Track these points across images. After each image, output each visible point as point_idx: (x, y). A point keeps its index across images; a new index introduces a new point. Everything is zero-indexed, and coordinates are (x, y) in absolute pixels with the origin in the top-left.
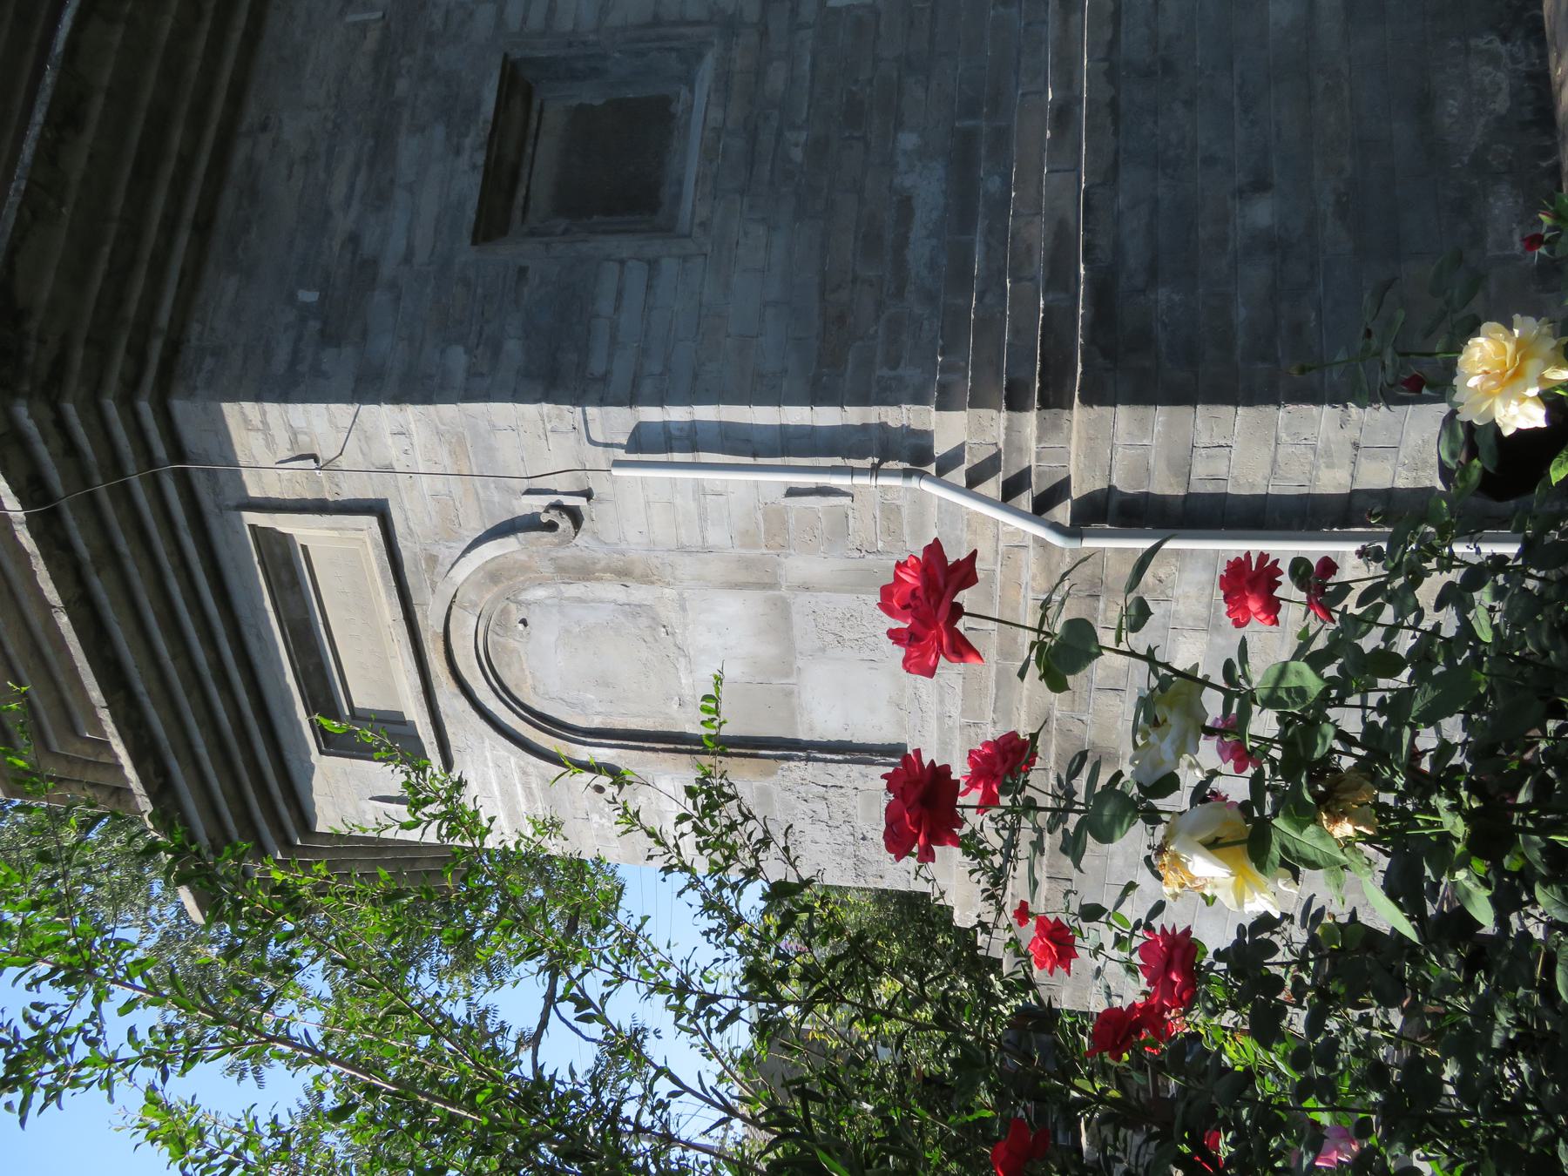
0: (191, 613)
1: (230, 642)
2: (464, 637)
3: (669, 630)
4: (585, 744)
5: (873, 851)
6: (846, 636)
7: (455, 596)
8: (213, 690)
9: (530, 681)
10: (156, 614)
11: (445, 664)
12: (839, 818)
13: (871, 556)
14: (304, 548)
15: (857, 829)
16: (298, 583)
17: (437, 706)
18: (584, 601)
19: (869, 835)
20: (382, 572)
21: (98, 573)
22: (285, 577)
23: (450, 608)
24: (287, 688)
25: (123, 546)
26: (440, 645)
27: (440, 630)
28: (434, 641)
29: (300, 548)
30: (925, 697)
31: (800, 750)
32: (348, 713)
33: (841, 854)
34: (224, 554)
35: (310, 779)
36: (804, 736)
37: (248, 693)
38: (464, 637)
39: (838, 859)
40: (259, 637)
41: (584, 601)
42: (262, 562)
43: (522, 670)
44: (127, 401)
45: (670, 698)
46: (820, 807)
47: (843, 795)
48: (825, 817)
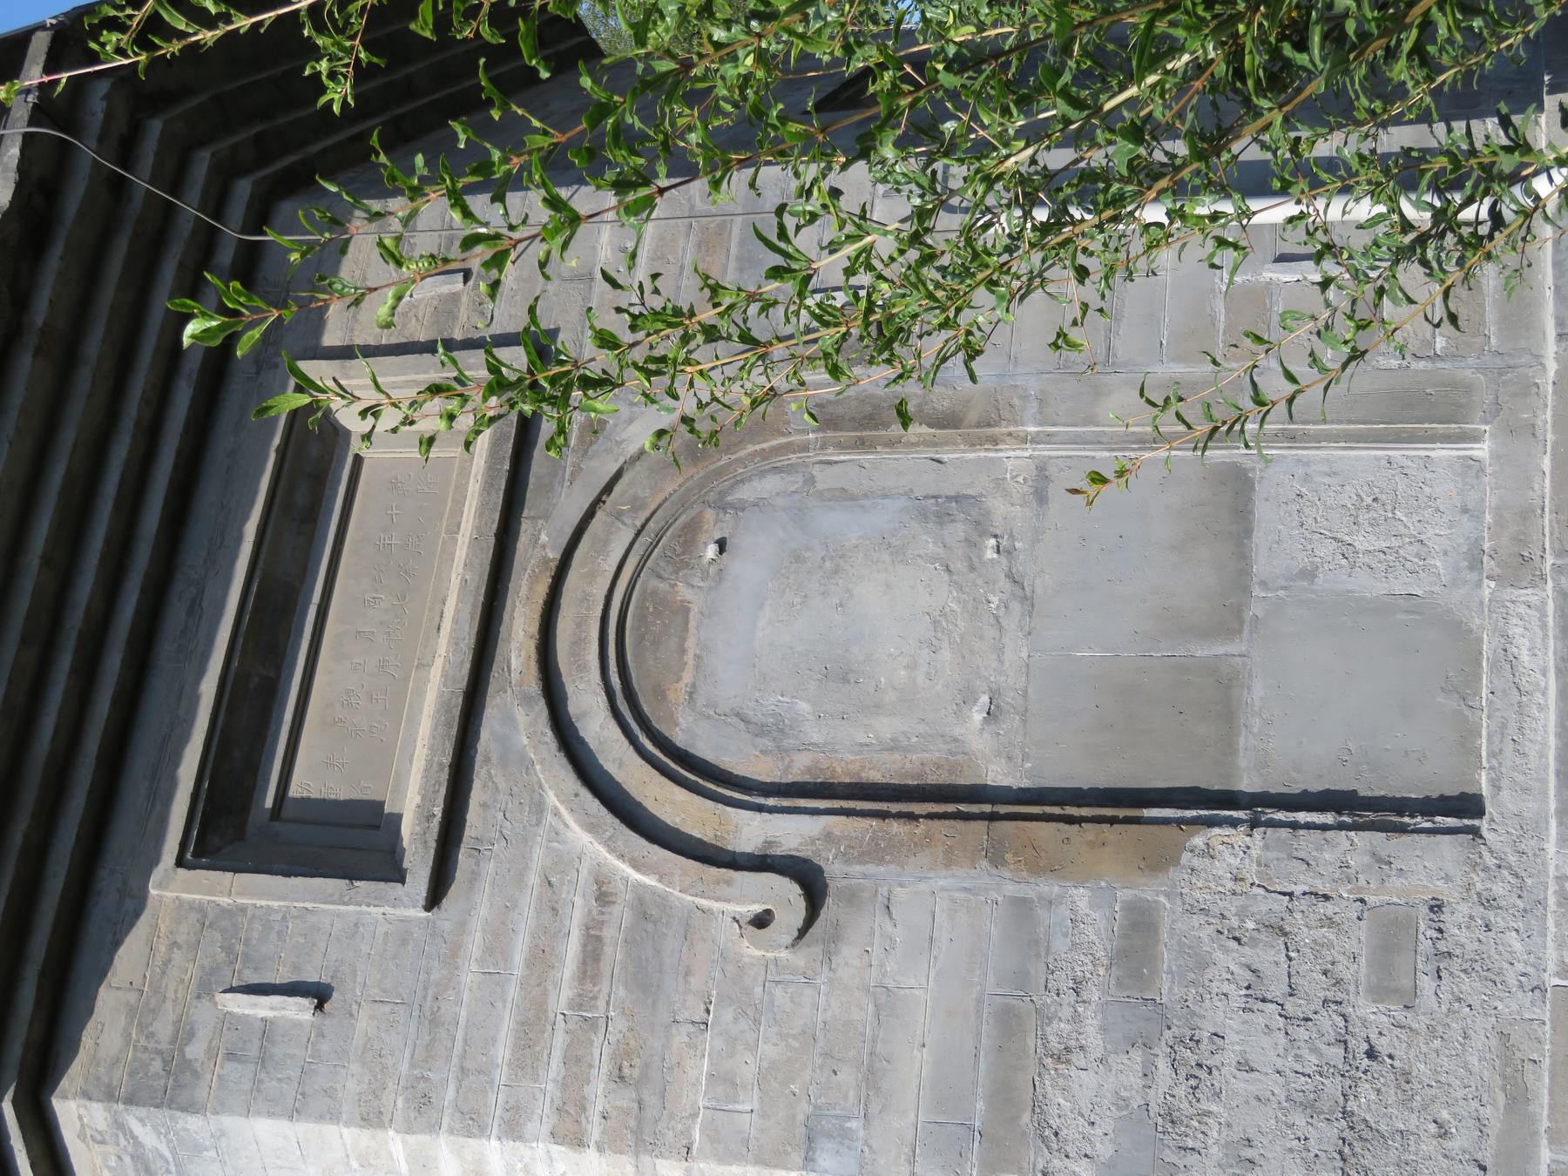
0: (117, 507)
1: (143, 591)
2: (591, 576)
3: (1004, 543)
4: (760, 809)
5: (1391, 1096)
6: (1360, 543)
7: (608, 488)
8: (65, 661)
9: (687, 677)
10: (69, 470)
11: (534, 629)
12: (1314, 984)
13: (1421, 365)
14: (358, 460)
15: (1357, 1028)
16: (315, 521)
17: (477, 737)
18: (853, 498)
19: (1382, 1045)
20: (444, 706)
21: (38, 351)
22: (301, 498)
23: (589, 515)
24: (195, 699)
25: (94, 345)
26: (542, 589)
27: (554, 555)
28: (534, 579)
29: (350, 460)
30: (1525, 658)
31: (1236, 807)
32: (269, 802)
33: (1310, 1107)
34: (223, 442)
35: (117, 944)
36: (1247, 784)
37: (114, 702)
38: (586, 598)
39: (1300, 1119)
40: (195, 607)
41: (853, 498)
42: (282, 452)
43: (683, 651)
44: (224, 176)
45: (968, 699)
46: (1269, 956)
47: (1329, 922)
48: (1278, 989)
